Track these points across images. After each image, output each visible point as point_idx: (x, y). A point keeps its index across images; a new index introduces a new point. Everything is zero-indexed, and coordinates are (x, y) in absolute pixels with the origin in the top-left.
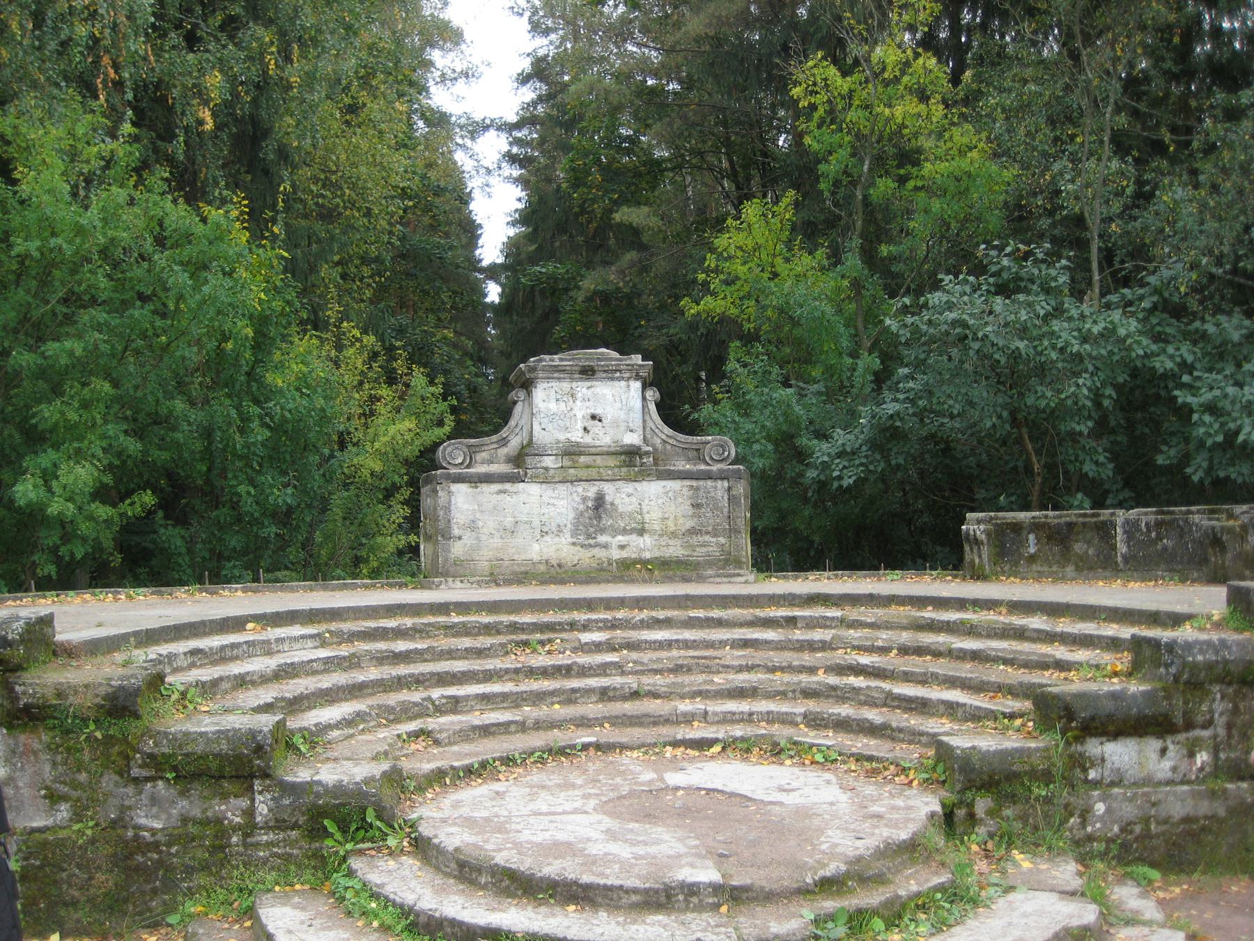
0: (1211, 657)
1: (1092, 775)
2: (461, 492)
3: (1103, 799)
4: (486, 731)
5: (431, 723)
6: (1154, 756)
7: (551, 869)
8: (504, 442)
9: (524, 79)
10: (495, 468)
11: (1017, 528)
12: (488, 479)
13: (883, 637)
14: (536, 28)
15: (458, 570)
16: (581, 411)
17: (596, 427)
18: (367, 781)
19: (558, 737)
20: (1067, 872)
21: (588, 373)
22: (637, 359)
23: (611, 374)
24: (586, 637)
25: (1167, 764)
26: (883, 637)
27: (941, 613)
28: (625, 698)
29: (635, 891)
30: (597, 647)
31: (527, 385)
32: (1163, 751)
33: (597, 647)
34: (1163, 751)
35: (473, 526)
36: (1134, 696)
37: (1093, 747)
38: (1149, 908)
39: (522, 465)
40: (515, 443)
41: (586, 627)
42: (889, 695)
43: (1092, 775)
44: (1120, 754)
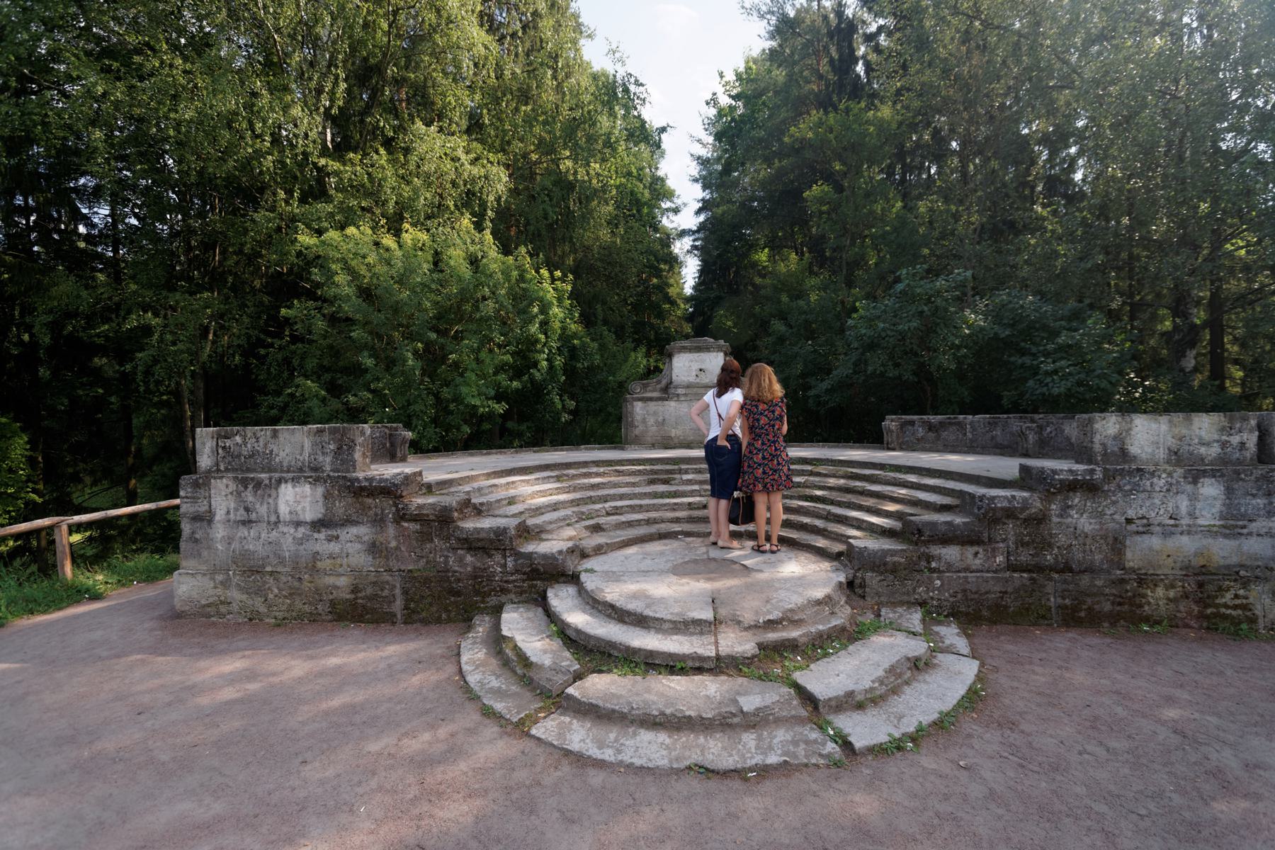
0: (1005, 504)
1: (934, 565)
2: (639, 405)
3: (938, 578)
4: (630, 524)
5: (602, 520)
6: (970, 557)
7: (631, 606)
8: (659, 382)
9: (698, 212)
10: (655, 394)
11: (912, 423)
12: (651, 399)
13: (832, 482)
14: (705, 188)
15: (638, 442)
16: (696, 366)
17: (702, 375)
18: (560, 552)
19: (664, 527)
20: (915, 619)
21: (699, 349)
22: (722, 342)
23: (707, 349)
24: (685, 477)
25: (978, 562)
26: (832, 482)
27: (496, 701)
28: (698, 508)
29: (670, 621)
30: (690, 482)
31: (670, 356)
32: (976, 554)
33: (690, 482)
34: (976, 554)
35: (644, 421)
36: (958, 525)
37: (936, 550)
38: (962, 644)
39: (667, 392)
40: (664, 382)
41: (686, 472)
42: (829, 512)
43: (934, 565)
44: (951, 553)
